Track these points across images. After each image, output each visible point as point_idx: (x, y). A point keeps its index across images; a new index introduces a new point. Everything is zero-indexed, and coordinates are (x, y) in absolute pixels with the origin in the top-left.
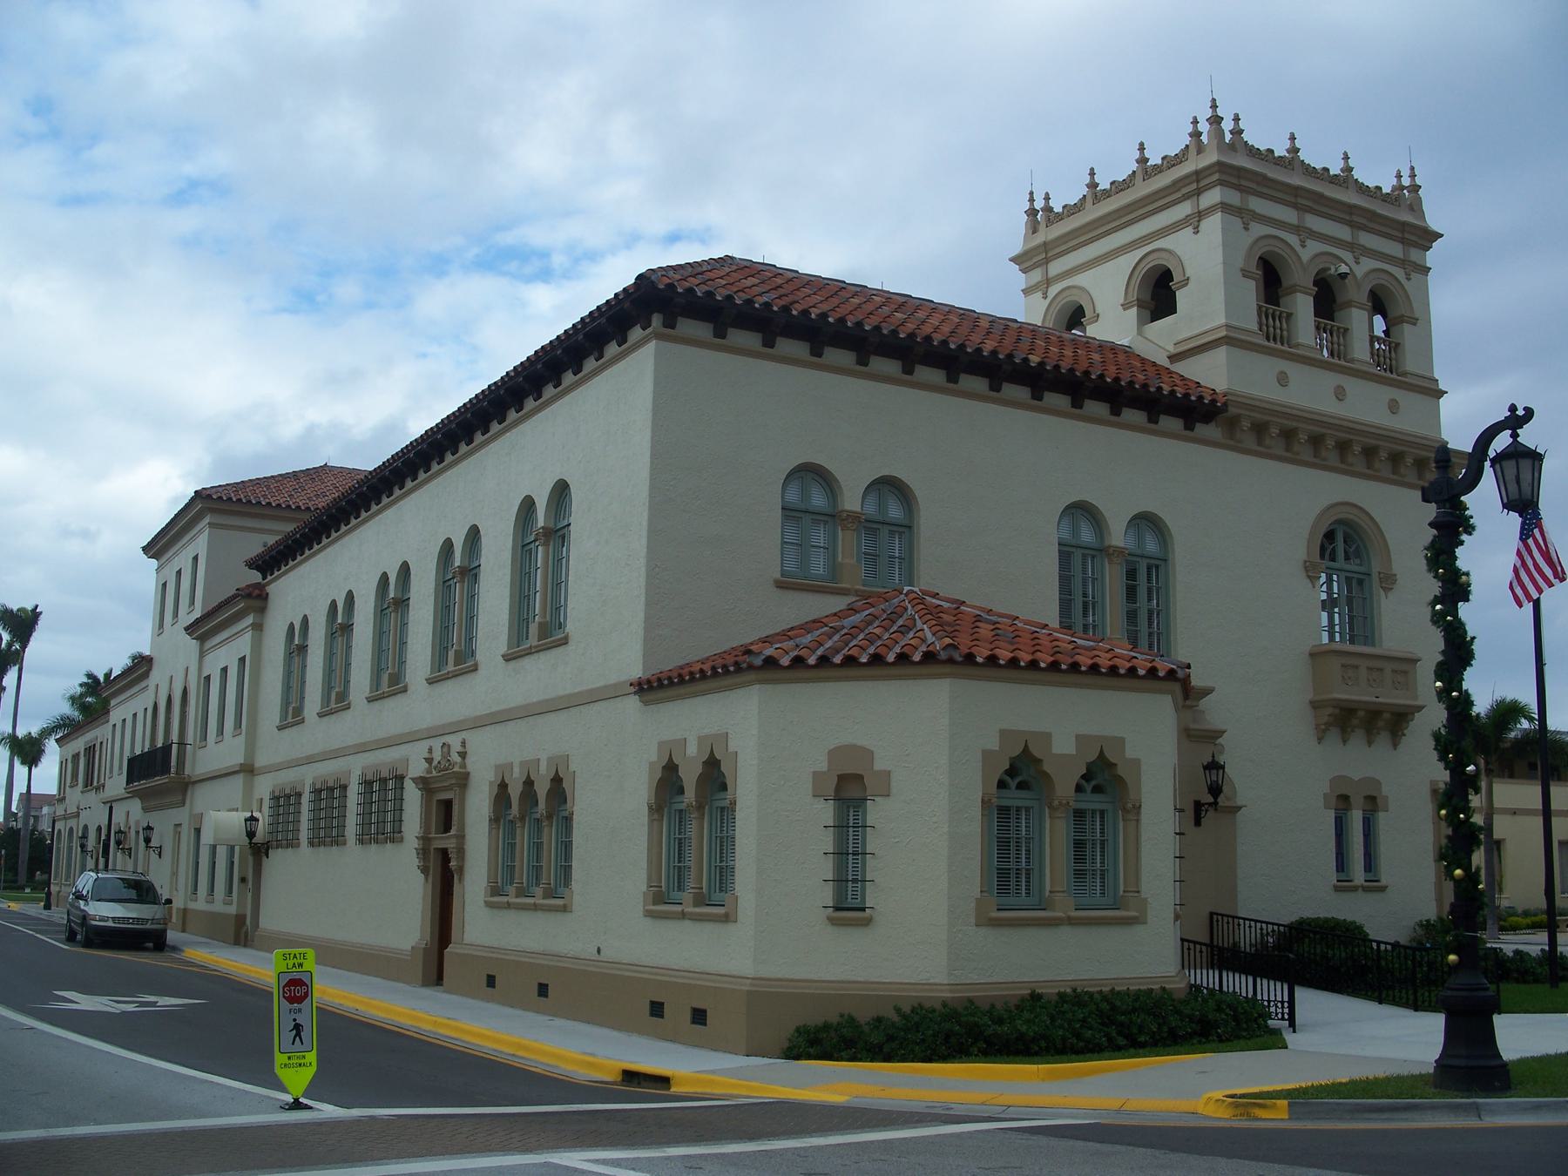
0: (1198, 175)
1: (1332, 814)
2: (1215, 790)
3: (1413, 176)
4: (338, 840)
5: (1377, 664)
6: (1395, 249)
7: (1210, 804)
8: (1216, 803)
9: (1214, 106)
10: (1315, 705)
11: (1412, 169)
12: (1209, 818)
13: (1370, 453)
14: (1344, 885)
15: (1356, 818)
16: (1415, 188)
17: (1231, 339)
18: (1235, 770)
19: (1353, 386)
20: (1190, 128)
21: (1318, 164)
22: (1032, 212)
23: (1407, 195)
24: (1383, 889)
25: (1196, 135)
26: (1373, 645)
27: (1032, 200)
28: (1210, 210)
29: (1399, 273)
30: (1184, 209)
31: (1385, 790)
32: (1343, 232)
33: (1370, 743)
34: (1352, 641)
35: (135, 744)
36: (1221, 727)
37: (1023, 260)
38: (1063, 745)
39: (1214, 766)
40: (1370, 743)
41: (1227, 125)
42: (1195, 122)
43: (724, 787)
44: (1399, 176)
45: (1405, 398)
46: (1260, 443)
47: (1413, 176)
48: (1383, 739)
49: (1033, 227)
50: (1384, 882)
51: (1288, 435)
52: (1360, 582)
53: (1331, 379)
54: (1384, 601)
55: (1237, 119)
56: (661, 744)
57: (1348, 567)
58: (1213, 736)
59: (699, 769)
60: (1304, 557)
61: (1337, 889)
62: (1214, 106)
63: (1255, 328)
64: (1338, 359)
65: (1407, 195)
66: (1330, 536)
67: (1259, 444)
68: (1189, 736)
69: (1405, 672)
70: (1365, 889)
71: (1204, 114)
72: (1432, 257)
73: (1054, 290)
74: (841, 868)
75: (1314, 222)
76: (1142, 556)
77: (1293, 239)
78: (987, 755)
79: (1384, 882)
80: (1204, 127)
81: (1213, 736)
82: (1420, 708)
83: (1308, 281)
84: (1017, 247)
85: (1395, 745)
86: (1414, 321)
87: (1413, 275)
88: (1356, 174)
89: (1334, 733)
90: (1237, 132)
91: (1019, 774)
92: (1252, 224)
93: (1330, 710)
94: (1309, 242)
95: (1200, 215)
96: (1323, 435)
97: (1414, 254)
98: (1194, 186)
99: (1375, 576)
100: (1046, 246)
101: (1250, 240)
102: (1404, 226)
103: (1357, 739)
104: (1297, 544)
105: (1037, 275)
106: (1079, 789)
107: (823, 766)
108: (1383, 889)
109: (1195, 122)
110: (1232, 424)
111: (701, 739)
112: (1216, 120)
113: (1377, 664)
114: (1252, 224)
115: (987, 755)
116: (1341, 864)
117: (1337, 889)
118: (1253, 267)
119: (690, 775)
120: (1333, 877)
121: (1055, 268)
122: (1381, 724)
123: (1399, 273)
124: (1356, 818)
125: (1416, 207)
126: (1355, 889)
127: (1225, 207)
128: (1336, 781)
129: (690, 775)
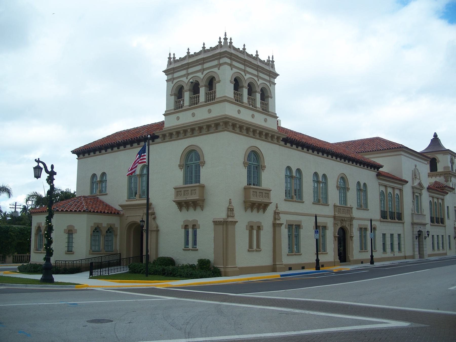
0: (220, 54)
3: (273, 58)
4: (296, 225)
5: (261, 191)
6: (267, 78)
9: (225, 35)
10: (245, 202)
11: (273, 56)
13: (248, 130)
14: (186, 248)
16: (273, 61)
19: (256, 114)
21: (250, 53)
22: (170, 58)
23: (270, 63)
24: (197, 250)
25: (220, 42)
27: (170, 55)
29: (268, 84)
30: (216, 62)
32: (255, 72)
33: (252, 212)
35: (21, 220)
37: (166, 72)
38: (105, 225)
40: (252, 212)
41: (229, 41)
42: (220, 38)
44: (269, 58)
45: (269, 118)
46: (233, 129)
47: (273, 58)
48: (261, 211)
49: (170, 63)
51: (241, 128)
53: (237, 108)
57: (253, 163)
62: (225, 35)
63: (233, 97)
64: (252, 106)
65: (270, 63)
67: (254, 135)
70: (192, 250)
71: (223, 37)
72: (276, 81)
73: (175, 81)
74: (68, 244)
75: (248, 69)
77: (256, 79)
80: (222, 40)
82: (271, 203)
83: (246, 85)
84: (165, 68)
86: (271, 97)
87: (272, 85)
88: (259, 57)
90: (231, 43)
94: (247, 75)
96: (274, 135)
97: (272, 80)
98: (219, 57)
99: (260, 166)
100: (174, 69)
102: (270, 72)
103: (255, 211)
104: (240, 157)
105: (170, 76)
106: (107, 232)
108: (197, 250)
112: (226, 39)
113: (261, 191)
114: (233, 69)
116: (187, 243)
118: (233, 80)
121: (176, 75)
122: (255, 206)
123: (268, 84)
124: (255, 232)
125: (273, 66)
126: (189, 250)
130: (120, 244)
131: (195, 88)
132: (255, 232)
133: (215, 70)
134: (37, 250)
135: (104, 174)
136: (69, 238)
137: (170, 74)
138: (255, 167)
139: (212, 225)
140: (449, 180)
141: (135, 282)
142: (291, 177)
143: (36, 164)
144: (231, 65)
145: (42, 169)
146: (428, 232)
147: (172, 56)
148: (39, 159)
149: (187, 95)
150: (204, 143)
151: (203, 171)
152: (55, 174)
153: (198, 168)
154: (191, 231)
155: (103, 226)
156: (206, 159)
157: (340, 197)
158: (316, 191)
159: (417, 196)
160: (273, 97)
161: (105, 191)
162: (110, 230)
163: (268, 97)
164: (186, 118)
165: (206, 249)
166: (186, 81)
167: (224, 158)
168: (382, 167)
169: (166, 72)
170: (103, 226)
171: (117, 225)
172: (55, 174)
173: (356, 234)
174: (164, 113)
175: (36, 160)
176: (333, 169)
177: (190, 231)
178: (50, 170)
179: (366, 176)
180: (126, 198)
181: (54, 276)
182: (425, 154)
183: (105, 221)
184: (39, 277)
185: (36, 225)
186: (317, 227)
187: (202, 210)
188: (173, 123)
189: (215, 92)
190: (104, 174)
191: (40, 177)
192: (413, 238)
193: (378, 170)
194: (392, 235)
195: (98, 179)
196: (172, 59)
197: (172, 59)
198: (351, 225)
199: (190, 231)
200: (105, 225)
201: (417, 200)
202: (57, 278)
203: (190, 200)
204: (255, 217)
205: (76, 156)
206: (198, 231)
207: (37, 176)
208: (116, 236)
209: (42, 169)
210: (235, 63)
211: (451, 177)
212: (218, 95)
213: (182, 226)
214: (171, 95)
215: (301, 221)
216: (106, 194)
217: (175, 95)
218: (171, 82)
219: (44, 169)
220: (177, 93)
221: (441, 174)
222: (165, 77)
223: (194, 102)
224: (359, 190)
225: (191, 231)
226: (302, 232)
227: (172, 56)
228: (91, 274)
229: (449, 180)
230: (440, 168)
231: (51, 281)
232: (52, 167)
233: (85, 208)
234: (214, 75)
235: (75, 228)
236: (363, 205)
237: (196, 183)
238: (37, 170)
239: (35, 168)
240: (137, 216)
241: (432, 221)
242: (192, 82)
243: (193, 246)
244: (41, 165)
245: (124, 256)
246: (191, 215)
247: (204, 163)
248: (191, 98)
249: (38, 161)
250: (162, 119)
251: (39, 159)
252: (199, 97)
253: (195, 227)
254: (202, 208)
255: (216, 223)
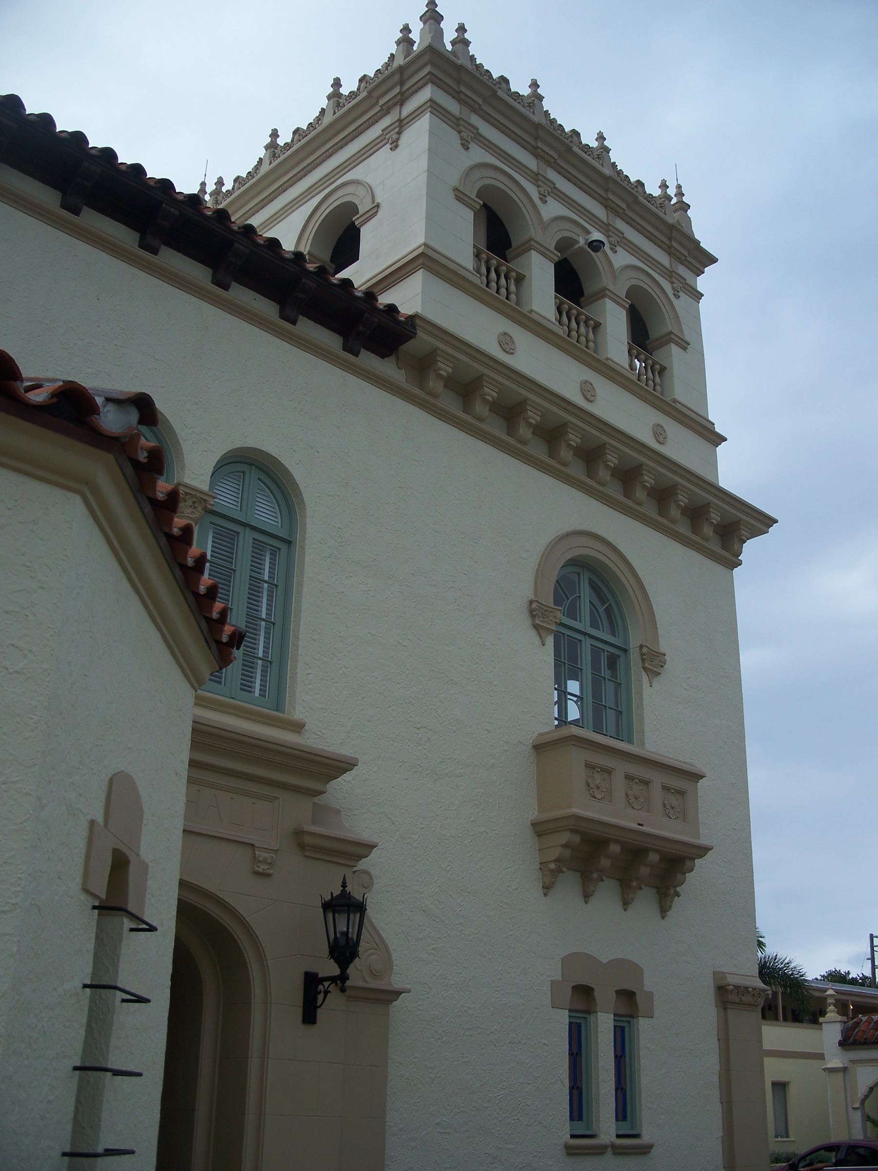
1: (564, 1017)
2: (344, 951)
7: (333, 979)
8: (343, 977)
12: (332, 1005)
15: (604, 1025)
17: (426, 261)
18: (385, 915)
24: (645, 1150)
26: (630, 741)
28: (416, 115)
31: (650, 982)
33: (626, 904)
34: (598, 728)
36: (366, 836)
39: (346, 905)
50: (646, 1138)
52: (613, 662)
54: (647, 691)
55: (462, 29)
58: (354, 851)
60: (530, 594)
61: (571, 1151)
68: (302, 847)
69: (681, 793)
70: (619, 1151)
76: (245, 525)
79: (646, 1138)
81: (354, 851)
85: (664, 911)
86: (684, 345)
89: (569, 882)
91: (787, 1137)
92: (472, 146)
93: (565, 837)
95: (402, 125)
99: (634, 655)
101: (469, 163)
103: (607, 896)
108: (645, 1150)
110: (422, 367)
114: (472, 146)
116: (579, 1106)
117: (571, 1151)
120: (563, 1129)
124: (604, 1025)
126: (600, 1151)
127: (433, 106)
128: (569, 961)
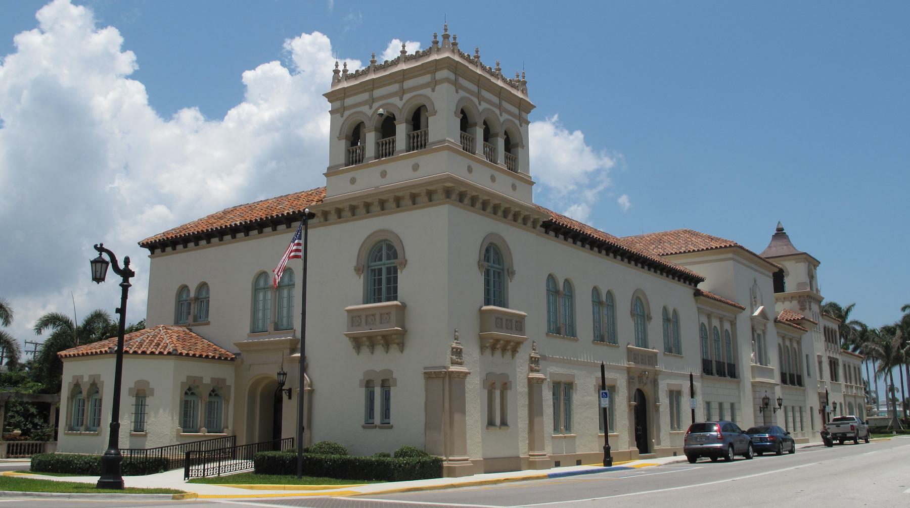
4: (565, 384)
9: (446, 30)
20: (433, 39)
22: (336, 72)
30: (427, 78)
38: (207, 380)
43: (97, 392)
45: (518, 183)
49: (336, 79)
56: (74, 377)
59: (89, 386)
66: (487, 250)
70: (380, 428)
75: (485, 94)
78: (182, 383)
80: (440, 39)
83: (480, 122)
97: (524, 114)
105: (338, 104)
106: (210, 395)
107: (133, 386)
109: (435, 37)
111: (90, 376)
115: (182, 383)
117: (364, 427)
119: (85, 390)
121: (349, 101)
124: (497, 393)
126: (375, 427)
129: (85, 390)
130: (236, 420)
131: (387, 126)
132: (497, 393)
133: (427, 92)
134: (71, 429)
135: (203, 286)
136: (137, 405)
137: (337, 99)
138: (496, 275)
139: (421, 382)
140: (807, 307)
141: (284, 489)
142: (557, 292)
143: (95, 255)
144: (455, 83)
145: (107, 263)
146: (779, 399)
147: (341, 68)
148: (101, 245)
149: (370, 139)
150: (399, 224)
151: (403, 278)
152: (132, 274)
153: (393, 273)
154: (378, 393)
155: (205, 381)
156: (409, 255)
157: (637, 331)
158: (597, 323)
159: (759, 335)
160: (525, 147)
161: (207, 316)
162: (216, 393)
163: (516, 146)
164: (370, 179)
165: (408, 424)
166: (371, 113)
167: (437, 252)
168: (702, 280)
169: (331, 96)
170: (205, 381)
171: (230, 382)
172: (132, 274)
173: (664, 401)
174: (325, 171)
175: (96, 247)
176: (624, 280)
177: (378, 391)
178: (121, 266)
179: (676, 296)
180: (247, 329)
181: (123, 478)
182: (770, 260)
183: (207, 373)
184: (94, 480)
185: (70, 380)
186: (603, 386)
187: (402, 352)
188: (346, 188)
189: (426, 134)
190: (203, 286)
191: (103, 279)
192: (755, 411)
193: (696, 286)
194: (721, 405)
195: (192, 294)
196: (341, 74)
197: (341, 74)
198: (655, 383)
199: (378, 391)
200: (207, 380)
201: (759, 342)
202: (129, 481)
203: (380, 333)
204: (498, 363)
205: (147, 252)
206: (393, 392)
207: (98, 278)
208: (228, 401)
209: (107, 263)
210: (462, 81)
211: (810, 302)
212: (431, 138)
213: (361, 381)
214: (339, 139)
215: (573, 376)
216: (208, 323)
217: (347, 138)
218: (339, 115)
219: (110, 265)
220: (352, 137)
221: (792, 298)
222: (329, 106)
223: (386, 150)
224: (666, 320)
225: (378, 393)
226: (577, 398)
227: (341, 68)
228: (187, 475)
229: (807, 307)
230: (790, 285)
231: (119, 486)
232: (127, 261)
233: (170, 348)
234: (423, 101)
235: (151, 386)
236: (673, 348)
237: (388, 300)
238: (99, 265)
239: (94, 262)
240: (267, 368)
241: (784, 381)
242: (381, 115)
243: (382, 419)
244: (106, 257)
245: (242, 441)
246: (378, 361)
247: (404, 263)
248: (377, 144)
249: (100, 249)
250: (322, 182)
251: (101, 245)
252: (394, 142)
253: (386, 385)
254: (402, 346)
255: (430, 376)
